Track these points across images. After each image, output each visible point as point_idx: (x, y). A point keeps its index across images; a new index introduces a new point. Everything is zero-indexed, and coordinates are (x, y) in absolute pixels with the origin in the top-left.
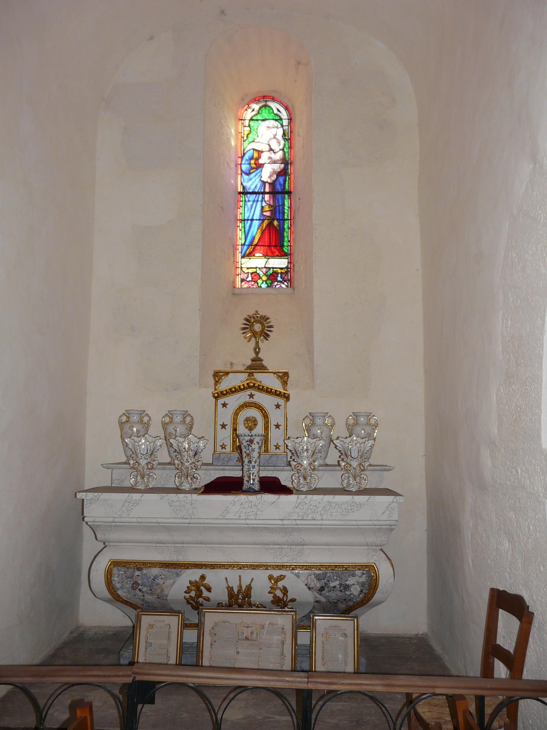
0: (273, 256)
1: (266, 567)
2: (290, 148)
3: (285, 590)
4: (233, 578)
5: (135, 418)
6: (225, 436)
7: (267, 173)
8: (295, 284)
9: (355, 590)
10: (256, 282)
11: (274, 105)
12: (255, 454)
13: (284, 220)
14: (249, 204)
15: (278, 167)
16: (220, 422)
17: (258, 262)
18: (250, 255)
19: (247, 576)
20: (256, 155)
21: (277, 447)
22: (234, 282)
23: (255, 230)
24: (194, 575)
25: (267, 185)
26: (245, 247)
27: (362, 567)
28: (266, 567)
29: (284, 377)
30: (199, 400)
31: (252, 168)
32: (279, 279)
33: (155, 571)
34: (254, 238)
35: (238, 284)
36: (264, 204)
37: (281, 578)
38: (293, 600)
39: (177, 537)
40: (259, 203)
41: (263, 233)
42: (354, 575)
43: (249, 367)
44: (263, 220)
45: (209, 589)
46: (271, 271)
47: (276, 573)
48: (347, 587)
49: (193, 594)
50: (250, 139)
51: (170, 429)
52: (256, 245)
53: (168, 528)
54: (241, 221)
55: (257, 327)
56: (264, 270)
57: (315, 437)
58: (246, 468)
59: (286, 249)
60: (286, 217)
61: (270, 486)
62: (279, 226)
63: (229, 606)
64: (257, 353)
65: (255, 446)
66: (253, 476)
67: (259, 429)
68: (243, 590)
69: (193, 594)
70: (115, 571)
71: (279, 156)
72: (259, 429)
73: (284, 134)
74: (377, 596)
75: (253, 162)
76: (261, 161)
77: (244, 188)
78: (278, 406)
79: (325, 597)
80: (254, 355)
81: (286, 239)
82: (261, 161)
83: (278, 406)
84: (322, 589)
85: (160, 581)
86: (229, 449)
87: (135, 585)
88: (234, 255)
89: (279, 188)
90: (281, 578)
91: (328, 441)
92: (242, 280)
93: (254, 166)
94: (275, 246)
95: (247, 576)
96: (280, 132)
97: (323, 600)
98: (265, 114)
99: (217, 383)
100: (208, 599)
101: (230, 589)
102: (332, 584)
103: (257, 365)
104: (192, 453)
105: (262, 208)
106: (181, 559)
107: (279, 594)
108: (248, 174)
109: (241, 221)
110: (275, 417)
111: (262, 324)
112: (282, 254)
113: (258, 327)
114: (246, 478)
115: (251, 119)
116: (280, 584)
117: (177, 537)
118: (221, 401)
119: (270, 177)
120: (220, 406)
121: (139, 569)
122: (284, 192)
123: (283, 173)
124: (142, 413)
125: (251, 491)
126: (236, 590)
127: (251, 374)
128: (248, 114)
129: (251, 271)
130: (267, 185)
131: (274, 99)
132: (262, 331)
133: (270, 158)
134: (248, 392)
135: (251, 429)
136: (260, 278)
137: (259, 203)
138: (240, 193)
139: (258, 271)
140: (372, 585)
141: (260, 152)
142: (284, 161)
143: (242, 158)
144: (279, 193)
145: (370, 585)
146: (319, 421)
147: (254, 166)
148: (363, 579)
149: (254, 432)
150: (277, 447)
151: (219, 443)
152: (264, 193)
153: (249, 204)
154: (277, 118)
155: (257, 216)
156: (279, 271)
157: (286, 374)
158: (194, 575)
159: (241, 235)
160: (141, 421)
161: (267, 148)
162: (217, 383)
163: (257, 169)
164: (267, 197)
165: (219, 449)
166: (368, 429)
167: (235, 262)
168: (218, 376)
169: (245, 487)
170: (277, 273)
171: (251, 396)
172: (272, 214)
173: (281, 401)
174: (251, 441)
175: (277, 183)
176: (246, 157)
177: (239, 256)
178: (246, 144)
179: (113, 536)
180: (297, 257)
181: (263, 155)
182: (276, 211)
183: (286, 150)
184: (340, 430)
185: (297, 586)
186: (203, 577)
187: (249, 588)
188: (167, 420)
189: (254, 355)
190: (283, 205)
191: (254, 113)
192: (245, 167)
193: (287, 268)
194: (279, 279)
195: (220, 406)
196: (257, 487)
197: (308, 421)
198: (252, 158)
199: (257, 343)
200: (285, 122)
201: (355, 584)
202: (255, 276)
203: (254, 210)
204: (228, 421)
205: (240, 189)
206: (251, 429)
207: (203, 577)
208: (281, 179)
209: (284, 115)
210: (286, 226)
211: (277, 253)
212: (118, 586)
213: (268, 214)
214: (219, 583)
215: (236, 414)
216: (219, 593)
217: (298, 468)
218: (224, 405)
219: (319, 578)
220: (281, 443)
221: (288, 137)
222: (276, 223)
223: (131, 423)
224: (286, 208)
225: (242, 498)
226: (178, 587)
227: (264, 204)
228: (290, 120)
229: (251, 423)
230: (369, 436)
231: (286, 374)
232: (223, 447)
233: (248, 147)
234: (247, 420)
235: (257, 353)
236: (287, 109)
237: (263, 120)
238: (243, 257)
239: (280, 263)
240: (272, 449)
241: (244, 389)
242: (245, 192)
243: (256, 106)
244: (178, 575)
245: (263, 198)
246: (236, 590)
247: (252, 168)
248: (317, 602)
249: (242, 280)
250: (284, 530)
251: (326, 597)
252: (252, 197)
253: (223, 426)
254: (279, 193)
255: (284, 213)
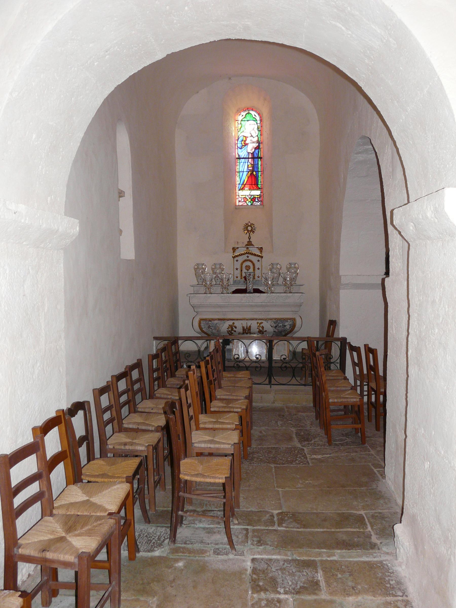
0: (254, 189)
1: (256, 319)
2: (261, 135)
3: (263, 327)
4: (244, 323)
5: (218, 266)
6: (238, 273)
7: (251, 148)
8: (264, 202)
9: (288, 327)
10: (246, 202)
11: (253, 113)
12: (252, 279)
13: (258, 171)
14: (242, 164)
15: (256, 145)
16: (235, 268)
17: (247, 192)
18: (243, 189)
19: (249, 323)
20: (244, 139)
21: (258, 277)
22: (236, 203)
23: (245, 177)
24: (231, 323)
25: (250, 154)
26: (240, 185)
27: (290, 319)
28: (256, 319)
29: (261, 249)
30: (226, 259)
31: (243, 146)
32: (256, 200)
33: (216, 322)
34: (244, 180)
35: (237, 204)
36: (249, 164)
37: (262, 323)
38: (266, 331)
39: (224, 310)
40: (246, 163)
41: (248, 178)
42: (287, 322)
43: (246, 245)
44: (248, 172)
45: (236, 328)
46: (253, 197)
47: (260, 321)
48: (285, 326)
49: (230, 329)
50: (241, 131)
51: (215, 270)
52: (245, 184)
53: (220, 306)
54: (238, 172)
55: (249, 228)
56: (249, 196)
57: (273, 273)
58: (248, 284)
59: (259, 186)
60: (259, 170)
61: (257, 291)
62: (256, 174)
63: (243, 333)
64: (250, 239)
65: (251, 276)
66: (251, 287)
67: (251, 270)
68: (177, 565)
69: (230, 329)
70: (202, 322)
71: (256, 139)
72: (251, 270)
73: (258, 128)
74: (296, 329)
75: (243, 142)
76: (247, 142)
77: (239, 156)
78: (258, 261)
79: (278, 330)
80: (248, 240)
81: (259, 181)
82: (247, 142)
83: (258, 261)
84: (276, 327)
85: (218, 325)
86: (239, 278)
87: (209, 327)
88: (236, 189)
89: (256, 156)
90: (262, 323)
91: (278, 275)
92: (239, 201)
93: (243, 144)
94: (254, 184)
95: (249, 323)
96: (256, 127)
97: (277, 331)
98: (248, 117)
99: (234, 252)
100: (235, 331)
101: (243, 327)
102: (280, 325)
103: (250, 243)
104: (227, 279)
105: (248, 165)
106: (225, 317)
107: (261, 329)
108: (241, 149)
109: (238, 172)
110: (257, 265)
111: (251, 227)
112: (258, 189)
113: (249, 228)
114: (248, 288)
115: (242, 120)
116: (261, 325)
117: (224, 310)
118: (236, 259)
119: (251, 150)
120: (235, 261)
121: (210, 321)
122: (258, 158)
123: (258, 148)
124: (220, 264)
125: (250, 293)
126: (245, 328)
127: (248, 248)
128: (240, 118)
129: (243, 197)
130: (250, 154)
131: (252, 110)
132: (251, 230)
133: (251, 140)
134: (247, 255)
135: (248, 270)
136: (248, 200)
137: (246, 163)
138: (237, 158)
139: (247, 197)
140: (293, 326)
141: (246, 137)
142: (258, 142)
143: (238, 140)
144: (256, 158)
145: (293, 326)
146: (275, 266)
147: (243, 144)
148: (291, 323)
149: (249, 271)
150: (258, 277)
151: (235, 276)
152: (249, 158)
153: (242, 164)
154: (255, 119)
155: (246, 170)
156: (256, 196)
157: (262, 248)
158: (231, 323)
159: (238, 179)
160: (220, 268)
161: (250, 135)
162: (234, 252)
163: (245, 146)
164: (250, 160)
165: (235, 278)
166: (295, 269)
167: (236, 193)
168: (234, 249)
169: (248, 291)
170: (256, 198)
171: (248, 257)
172: (253, 168)
173: (260, 259)
174: (250, 275)
175: (255, 153)
176: (240, 140)
177: (237, 189)
178: (239, 133)
179: (200, 310)
180: (264, 191)
181: (248, 139)
182: (254, 166)
183: (259, 136)
184: (284, 270)
185: (268, 326)
186: (234, 323)
187: (250, 327)
188: (213, 267)
189: (248, 240)
190: (258, 164)
191: (243, 117)
192: (239, 145)
193: (260, 195)
194: (256, 200)
195: (235, 261)
196: (252, 291)
197: (271, 267)
198: (243, 140)
199: (250, 235)
200: (259, 122)
201: (288, 325)
202: (245, 199)
203: (243, 167)
204: (239, 267)
205: (237, 156)
206: (248, 270)
207: (234, 323)
208: (257, 151)
209: (258, 118)
210: (259, 175)
211: (255, 188)
212: (203, 327)
213: (251, 169)
214: (239, 326)
215: (242, 264)
216: (239, 329)
217: (267, 285)
218: (237, 261)
219: (275, 323)
220: (260, 276)
221: (260, 129)
222: (254, 173)
223: (198, 270)
224: (259, 165)
225: (247, 295)
226: (224, 327)
227: (249, 164)
228: (261, 120)
229: (248, 268)
230: (295, 272)
231: (262, 248)
232: (237, 277)
233: (241, 134)
234: (246, 266)
235: (250, 239)
236: (259, 114)
237: (248, 121)
238: (239, 190)
239: (257, 193)
240: (256, 278)
241: (245, 254)
242: (240, 158)
243: (244, 114)
244: (225, 323)
245: (248, 161)
246: (245, 328)
247: (243, 146)
248: (274, 331)
249: (239, 201)
250: (262, 306)
251: (278, 330)
252: (243, 160)
253: (237, 269)
254: (256, 158)
255: (258, 168)
